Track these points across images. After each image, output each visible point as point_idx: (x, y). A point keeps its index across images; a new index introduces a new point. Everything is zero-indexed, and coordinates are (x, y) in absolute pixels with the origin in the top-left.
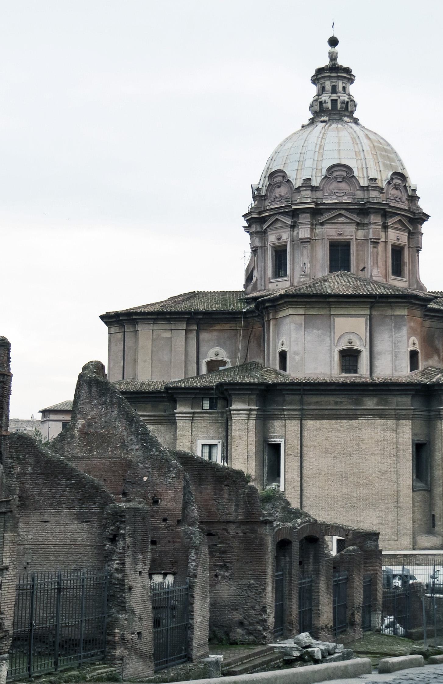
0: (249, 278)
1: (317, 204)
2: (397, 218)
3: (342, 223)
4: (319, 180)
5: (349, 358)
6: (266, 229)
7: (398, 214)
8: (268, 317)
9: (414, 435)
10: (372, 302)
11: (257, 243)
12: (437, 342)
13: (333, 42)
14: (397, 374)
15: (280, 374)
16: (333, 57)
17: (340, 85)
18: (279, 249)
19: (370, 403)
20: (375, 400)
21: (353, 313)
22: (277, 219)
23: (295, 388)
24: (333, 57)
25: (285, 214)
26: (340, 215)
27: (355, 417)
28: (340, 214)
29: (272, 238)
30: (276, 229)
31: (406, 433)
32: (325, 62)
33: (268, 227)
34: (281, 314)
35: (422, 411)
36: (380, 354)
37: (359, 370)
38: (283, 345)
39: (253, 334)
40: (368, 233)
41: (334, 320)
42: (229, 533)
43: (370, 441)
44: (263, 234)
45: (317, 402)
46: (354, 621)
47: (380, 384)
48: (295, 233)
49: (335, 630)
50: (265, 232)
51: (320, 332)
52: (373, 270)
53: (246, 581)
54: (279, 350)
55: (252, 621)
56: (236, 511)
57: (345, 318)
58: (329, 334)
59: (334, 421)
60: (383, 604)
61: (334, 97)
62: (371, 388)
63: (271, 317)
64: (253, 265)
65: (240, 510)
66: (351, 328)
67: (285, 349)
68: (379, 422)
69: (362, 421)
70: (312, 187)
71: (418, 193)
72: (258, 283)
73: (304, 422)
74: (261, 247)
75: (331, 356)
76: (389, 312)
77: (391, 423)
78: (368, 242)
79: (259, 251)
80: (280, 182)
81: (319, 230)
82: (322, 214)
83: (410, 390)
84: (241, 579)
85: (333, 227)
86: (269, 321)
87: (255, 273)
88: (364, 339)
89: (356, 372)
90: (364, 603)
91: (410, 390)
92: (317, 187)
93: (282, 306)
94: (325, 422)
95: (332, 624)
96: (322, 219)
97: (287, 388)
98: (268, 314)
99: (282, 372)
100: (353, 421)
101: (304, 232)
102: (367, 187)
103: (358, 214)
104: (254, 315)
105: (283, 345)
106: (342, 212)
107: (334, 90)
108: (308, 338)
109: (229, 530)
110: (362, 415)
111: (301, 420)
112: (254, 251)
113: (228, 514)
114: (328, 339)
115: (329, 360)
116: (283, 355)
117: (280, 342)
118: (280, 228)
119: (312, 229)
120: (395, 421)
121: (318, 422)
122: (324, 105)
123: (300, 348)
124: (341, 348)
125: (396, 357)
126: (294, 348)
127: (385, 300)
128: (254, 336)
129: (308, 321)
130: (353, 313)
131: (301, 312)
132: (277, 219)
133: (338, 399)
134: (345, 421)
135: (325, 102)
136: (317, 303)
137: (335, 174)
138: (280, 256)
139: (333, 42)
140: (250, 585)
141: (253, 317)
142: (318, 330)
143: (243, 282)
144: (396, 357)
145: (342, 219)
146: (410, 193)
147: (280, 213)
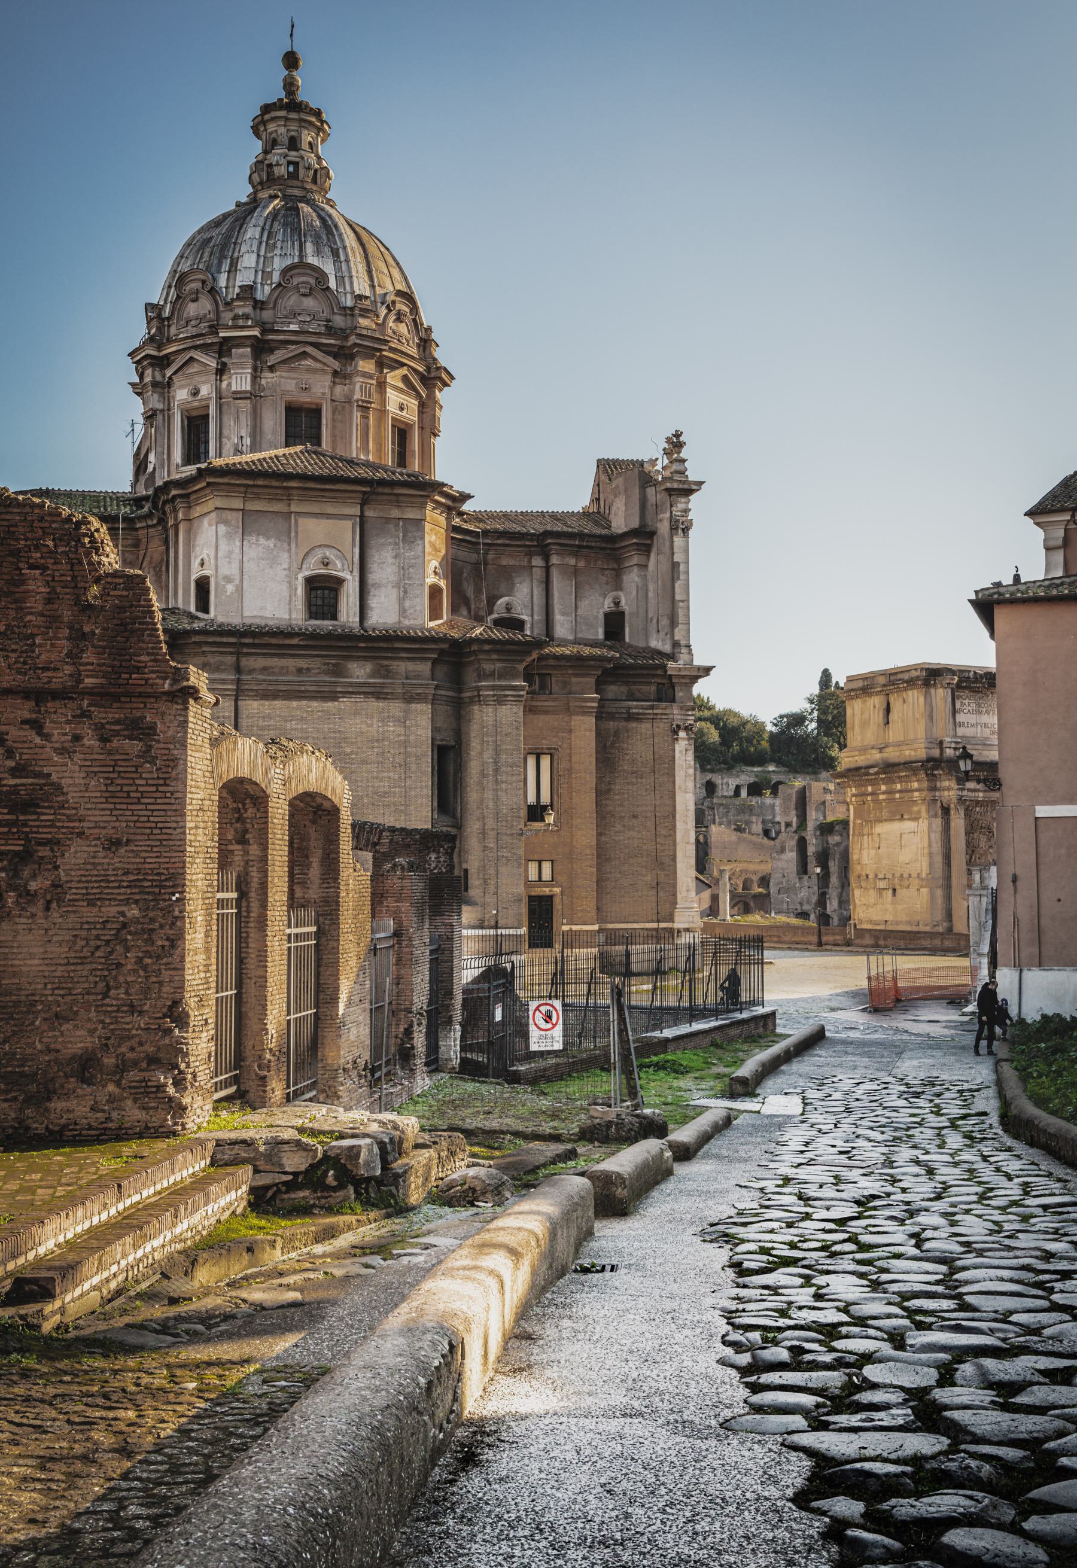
0: (140, 466)
1: (264, 332)
2: (404, 371)
3: (309, 370)
4: (267, 289)
5: (322, 592)
6: (170, 378)
7: (403, 365)
8: (176, 519)
9: (435, 730)
10: (365, 493)
11: (155, 402)
12: (465, 584)
13: (291, 60)
14: (407, 622)
15: (197, 618)
16: (290, 86)
17: (307, 137)
18: (194, 414)
19: (360, 671)
20: (368, 667)
21: (330, 510)
22: (192, 359)
23: (225, 640)
24: (290, 86)
25: (205, 348)
26: (304, 355)
27: (333, 696)
28: (304, 353)
29: (181, 395)
30: (189, 376)
31: (420, 724)
32: (277, 93)
33: (175, 373)
34: (198, 511)
35: (449, 689)
36: (378, 586)
37: (339, 615)
38: (202, 564)
39: (147, 559)
40: (352, 392)
41: (296, 522)
42: (47, 737)
43: (359, 740)
44: (164, 387)
45: (265, 669)
46: (413, 1048)
47: (379, 639)
48: (224, 384)
49: (373, 1071)
50: (169, 384)
51: (271, 543)
52: (367, 448)
53: (111, 911)
54: (194, 577)
55: (130, 1055)
56: (74, 656)
57: (314, 520)
58: (285, 545)
59: (295, 704)
60: (463, 1005)
61: (293, 155)
62: (362, 645)
63: (180, 516)
64: (148, 444)
65: (89, 656)
66: (327, 537)
67: (206, 572)
68: (374, 704)
69: (345, 702)
70: (256, 301)
71: (434, 336)
72: (157, 475)
73: (240, 703)
74: (162, 411)
75: (292, 589)
76: (395, 513)
77: (395, 708)
78: (351, 406)
79: (160, 417)
80: (198, 292)
81: (268, 379)
82: (272, 351)
83: (432, 650)
84: (91, 903)
85: (292, 375)
86: (176, 527)
87: (152, 458)
88: (349, 557)
89: (334, 617)
90: (429, 1004)
91: (432, 650)
92: (263, 302)
93: (202, 493)
94: (278, 704)
95: (366, 1056)
96: (272, 360)
97: (210, 640)
98: (175, 511)
99: (200, 615)
100: (330, 704)
101: (240, 381)
102: (352, 309)
103: (335, 356)
104: (150, 523)
105: (202, 564)
106: (309, 349)
107: (293, 144)
108: (251, 552)
109: (48, 727)
110: (345, 694)
111: (236, 701)
112: (150, 417)
113: (45, 669)
114: (286, 555)
115: (286, 593)
116: (203, 587)
117: (198, 561)
118: (196, 374)
119: (255, 378)
120: (403, 706)
121: (267, 703)
122: (276, 169)
123: (233, 570)
124: (307, 573)
125: (405, 592)
126: (225, 570)
127: (387, 490)
128: (150, 563)
129: (248, 523)
130: (330, 510)
131: (238, 504)
132: (192, 359)
133: (303, 663)
134: (315, 704)
135: (278, 165)
136: (263, 492)
137: (296, 281)
138: (196, 427)
139: (291, 60)
140: (124, 925)
141: (148, 527)
142: (268, 538)
143: (130, 477)
144: (405, 592)
145: (309, 362)
146: (423, 335)
147: (196, 347)
